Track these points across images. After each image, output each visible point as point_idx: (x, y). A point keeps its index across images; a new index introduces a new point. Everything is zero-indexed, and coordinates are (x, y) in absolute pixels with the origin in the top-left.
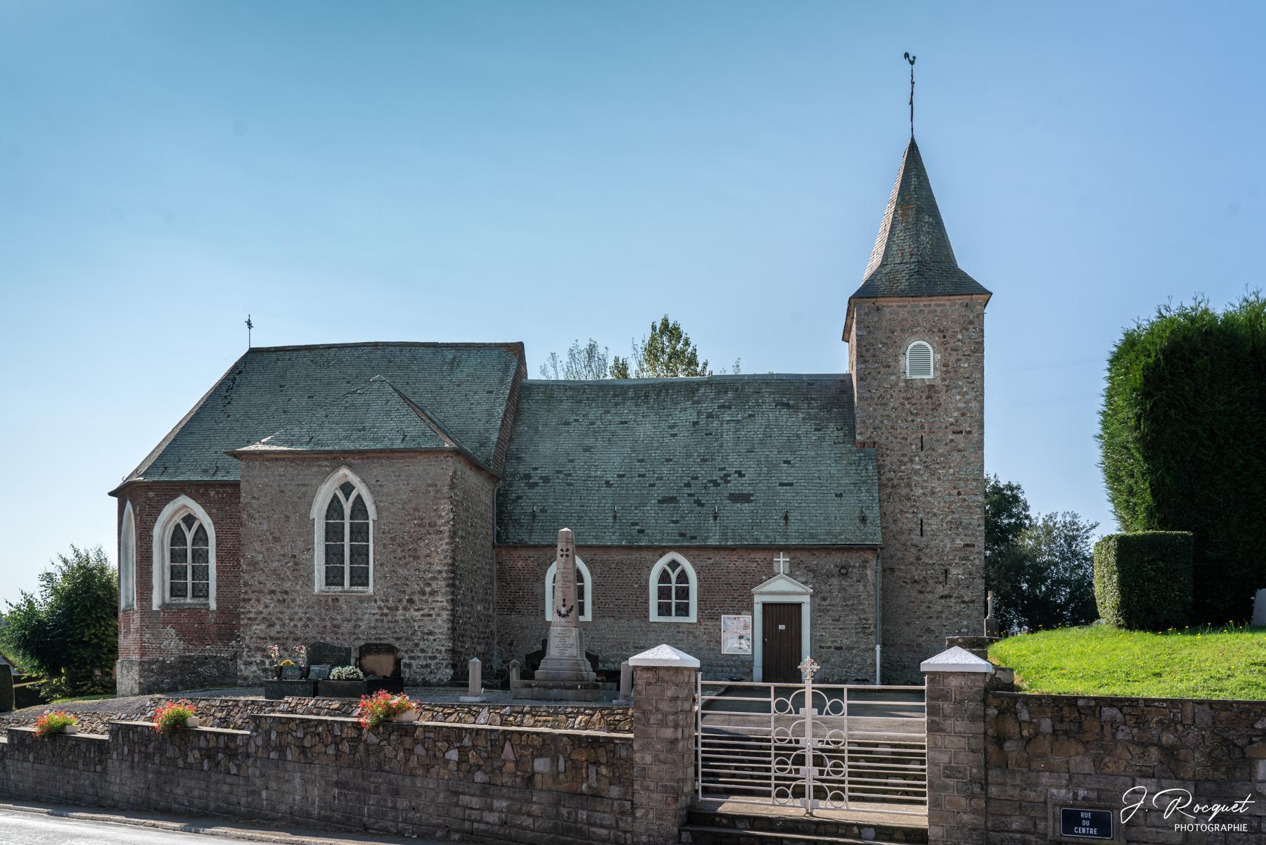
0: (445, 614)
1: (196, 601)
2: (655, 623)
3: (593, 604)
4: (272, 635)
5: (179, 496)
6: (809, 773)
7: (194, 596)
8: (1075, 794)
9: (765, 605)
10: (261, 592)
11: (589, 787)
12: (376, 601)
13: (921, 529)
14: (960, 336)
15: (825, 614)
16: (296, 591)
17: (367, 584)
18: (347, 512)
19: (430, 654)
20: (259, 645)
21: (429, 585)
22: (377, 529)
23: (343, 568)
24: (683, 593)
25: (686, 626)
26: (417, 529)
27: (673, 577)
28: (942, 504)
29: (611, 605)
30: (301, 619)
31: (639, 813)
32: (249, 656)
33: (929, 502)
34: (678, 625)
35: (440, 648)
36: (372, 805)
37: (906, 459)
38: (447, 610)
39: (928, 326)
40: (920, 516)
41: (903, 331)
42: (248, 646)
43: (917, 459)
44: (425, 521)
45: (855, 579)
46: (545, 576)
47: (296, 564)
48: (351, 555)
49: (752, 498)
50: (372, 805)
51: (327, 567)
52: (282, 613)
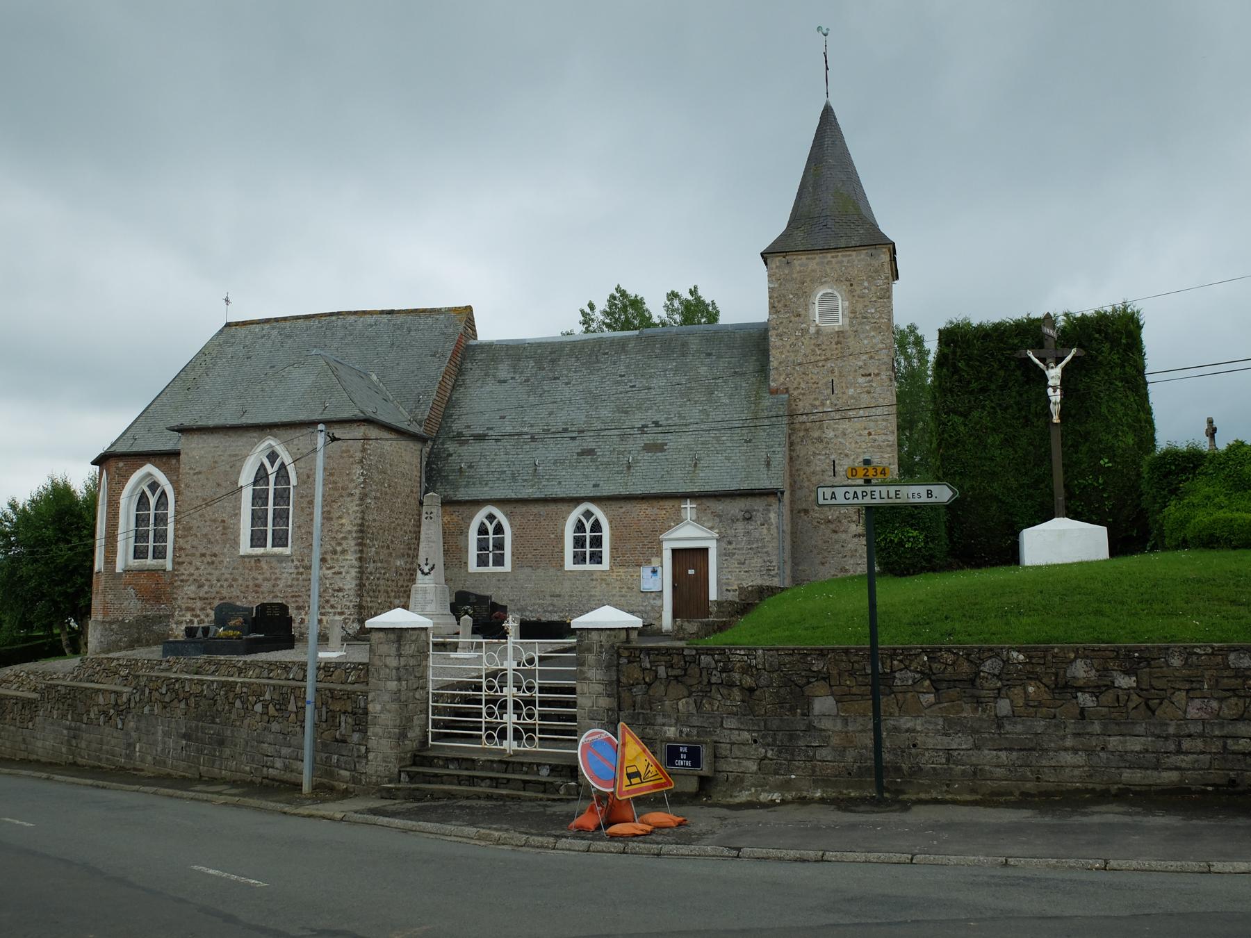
0: (353, 572)
1: (155, 562)
2: (571, 571)
3: (513, 555)
4: (201, 596)
5: (145, 464)
6: (510, 719)
7: (154, 558)
8: (681, 732)
9: (674, 551)
10: (193, 555)
11: (340, 734)
12: (293, 561)
13: (834, 470)
14: (866, 284)
15: (731, 558)
16: (223, 554)
17: (287, 546)
18: (272, 478)
19: (339, 610)
20: (190, 605)
21: (340, 544)
22: (297, 494)
23: (266, 530)
24: (597, 542)
25: (598, 574)
26: (332, 492)
27: (588, 526)
28: (853, 445)
29: (529, 556)
30: (226, 580)
31: (371, 756)
32: (180, 616)
33: (840, 443)
34: (591, 573)
35: (348, 604)
36: (207, 754)
37: (817, 403)
38: (356, 567)
39: (836, 276)
40: (833, 457)
41: (812, 281)
42: (179, 607)
43: (828, 402)
44: (339, 485)
45: (759, 522)
46: (468, 529)
47: (224, 528)
48: (274, 519)
49: (665, 447)
50: (207, 754)
51: (252, 530)
52: (210, 574)
